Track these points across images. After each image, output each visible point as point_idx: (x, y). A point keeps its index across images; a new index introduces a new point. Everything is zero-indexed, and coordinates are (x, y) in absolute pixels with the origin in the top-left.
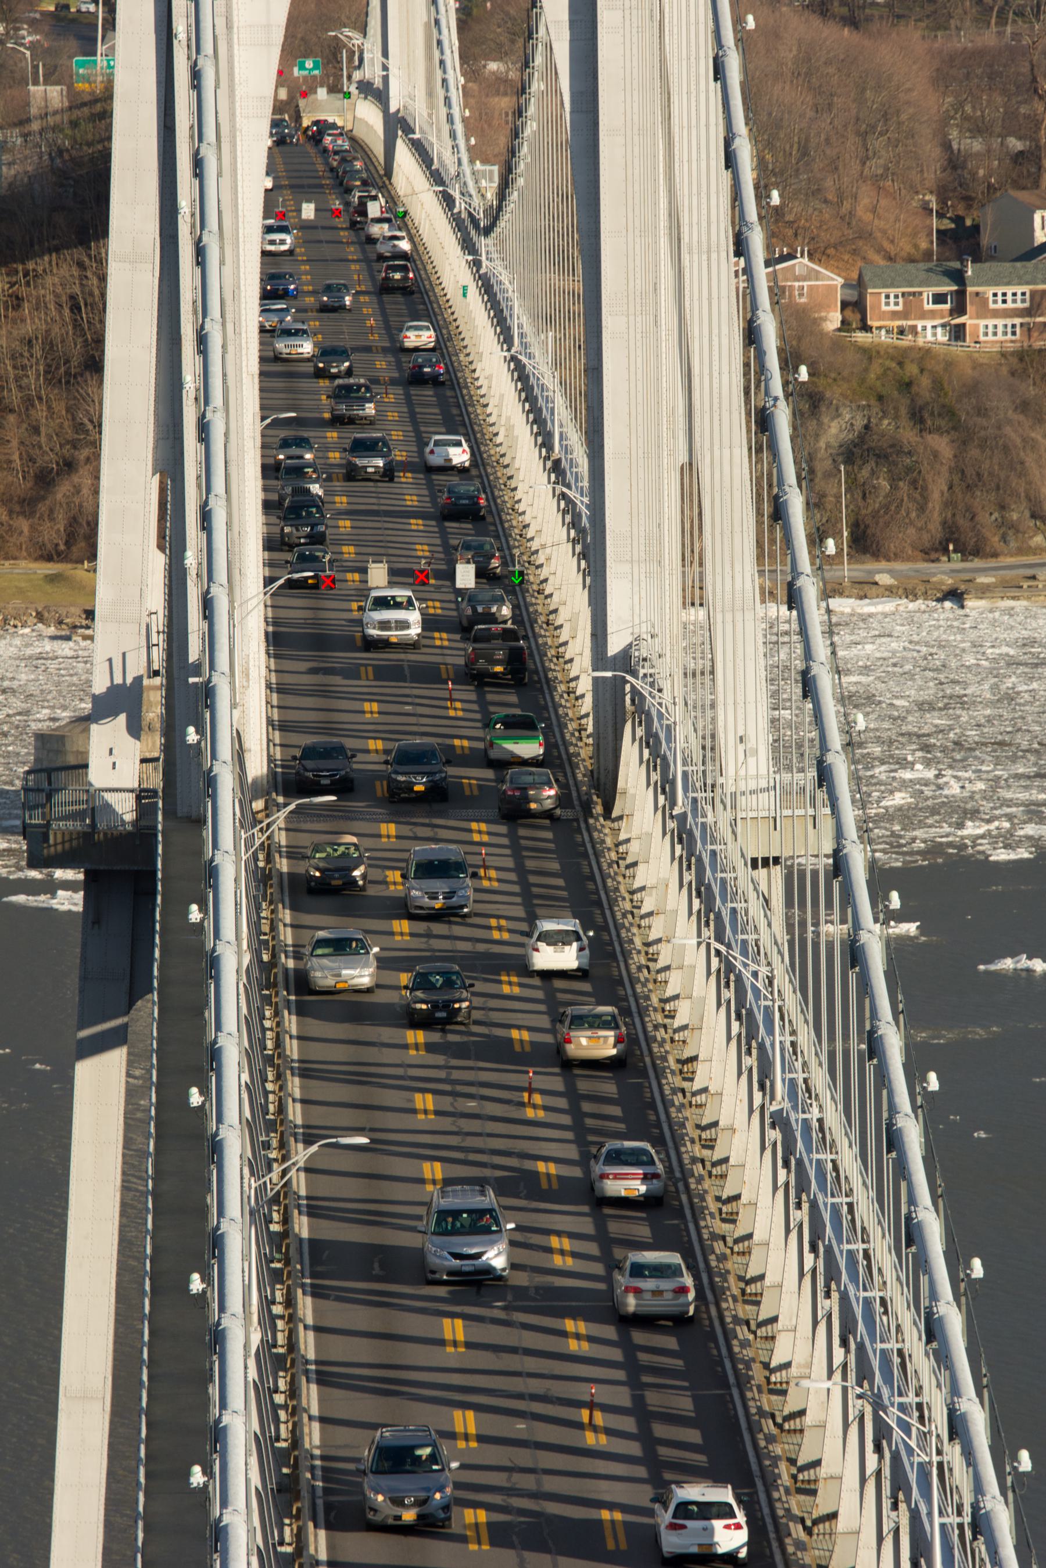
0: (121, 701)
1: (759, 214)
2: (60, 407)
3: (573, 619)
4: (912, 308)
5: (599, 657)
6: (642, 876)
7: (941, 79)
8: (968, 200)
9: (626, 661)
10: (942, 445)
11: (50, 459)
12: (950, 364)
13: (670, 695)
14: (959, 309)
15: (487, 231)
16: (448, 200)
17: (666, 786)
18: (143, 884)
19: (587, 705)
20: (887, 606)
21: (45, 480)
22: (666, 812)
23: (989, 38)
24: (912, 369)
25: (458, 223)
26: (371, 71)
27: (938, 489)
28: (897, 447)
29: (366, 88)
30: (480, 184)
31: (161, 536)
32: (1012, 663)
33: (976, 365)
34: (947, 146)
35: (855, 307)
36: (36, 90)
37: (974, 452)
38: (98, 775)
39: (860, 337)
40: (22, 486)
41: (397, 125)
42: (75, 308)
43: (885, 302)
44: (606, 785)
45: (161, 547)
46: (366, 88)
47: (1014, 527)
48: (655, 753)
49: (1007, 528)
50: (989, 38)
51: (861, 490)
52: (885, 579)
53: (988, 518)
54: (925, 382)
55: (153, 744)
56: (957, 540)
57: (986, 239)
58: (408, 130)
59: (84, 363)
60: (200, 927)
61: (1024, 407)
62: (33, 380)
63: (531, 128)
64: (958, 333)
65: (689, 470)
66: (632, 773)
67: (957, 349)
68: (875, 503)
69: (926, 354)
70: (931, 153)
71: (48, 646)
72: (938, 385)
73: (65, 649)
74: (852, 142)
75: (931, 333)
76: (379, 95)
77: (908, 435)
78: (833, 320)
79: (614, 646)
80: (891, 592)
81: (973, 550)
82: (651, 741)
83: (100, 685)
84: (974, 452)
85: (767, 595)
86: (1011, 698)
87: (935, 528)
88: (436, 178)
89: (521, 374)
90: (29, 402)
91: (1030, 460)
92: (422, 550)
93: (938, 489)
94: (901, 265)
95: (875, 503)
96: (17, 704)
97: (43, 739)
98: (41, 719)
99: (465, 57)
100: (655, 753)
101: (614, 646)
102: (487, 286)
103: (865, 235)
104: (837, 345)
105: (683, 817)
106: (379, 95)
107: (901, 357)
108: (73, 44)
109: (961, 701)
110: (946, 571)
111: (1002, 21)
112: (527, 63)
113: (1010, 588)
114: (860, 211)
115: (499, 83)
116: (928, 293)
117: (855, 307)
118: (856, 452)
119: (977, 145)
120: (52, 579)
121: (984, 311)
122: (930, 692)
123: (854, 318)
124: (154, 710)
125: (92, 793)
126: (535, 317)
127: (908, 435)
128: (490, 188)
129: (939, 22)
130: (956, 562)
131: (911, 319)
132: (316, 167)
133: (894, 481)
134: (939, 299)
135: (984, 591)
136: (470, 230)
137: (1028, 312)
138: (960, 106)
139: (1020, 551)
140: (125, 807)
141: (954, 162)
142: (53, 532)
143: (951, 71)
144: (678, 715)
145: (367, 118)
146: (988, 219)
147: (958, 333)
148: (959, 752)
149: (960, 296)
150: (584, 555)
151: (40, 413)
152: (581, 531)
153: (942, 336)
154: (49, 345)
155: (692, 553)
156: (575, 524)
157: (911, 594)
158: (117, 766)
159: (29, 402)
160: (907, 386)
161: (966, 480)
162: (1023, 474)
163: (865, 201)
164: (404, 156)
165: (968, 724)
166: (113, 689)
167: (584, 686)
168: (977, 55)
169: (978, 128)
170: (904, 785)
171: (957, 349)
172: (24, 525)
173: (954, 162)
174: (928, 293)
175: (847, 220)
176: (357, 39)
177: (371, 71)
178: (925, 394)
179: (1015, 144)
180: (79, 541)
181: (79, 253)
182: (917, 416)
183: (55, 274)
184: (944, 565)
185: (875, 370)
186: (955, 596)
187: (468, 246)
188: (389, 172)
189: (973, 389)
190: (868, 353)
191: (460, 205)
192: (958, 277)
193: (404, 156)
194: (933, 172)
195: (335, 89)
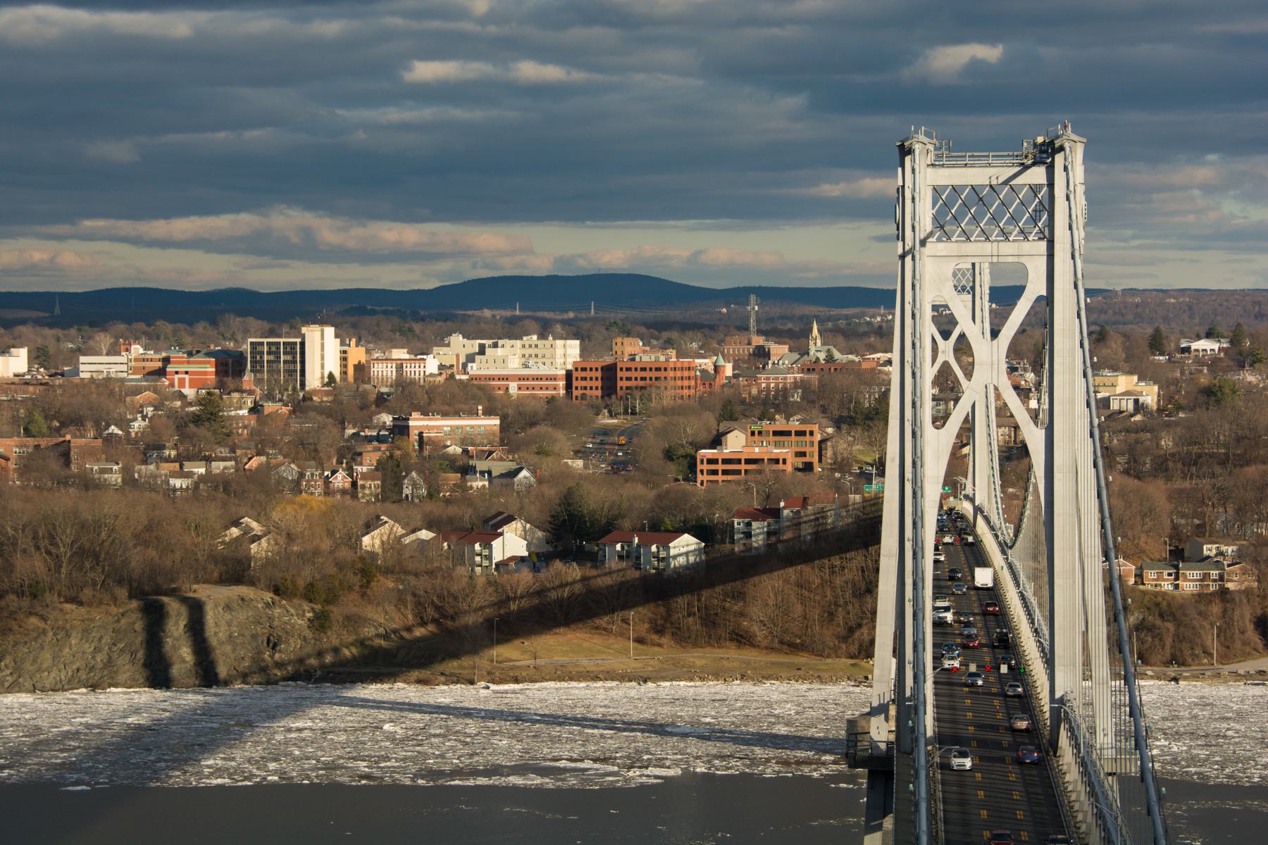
0: (882, 709)
1: (28, 691)
2: (857, 605)
3: (1042, 685)
4: (1160, 578)
5: (1052, 699)
6: (1068, 778)
7: (1170, 498)
8: (1180, 541)
9: (1062, 701)
10: (1170, 626)
11: (853, 624)
12: (1173, 598)
13: (1078, 710)
14: (1177, 578)
15: (1011, 548)
16: (996, 536)
17: (1077, 746)
18: (889, 775)
19: (1047, 715)
20: (1151, 682)
21: (851, 630)
22: (1077, 755)
23: (1187, 484)
24: (1160, 599)
25: (1000, 544)
26: (969, 491)
27: (1169, 641)
28: (1154, 626)
29: (966, 497)
30: (1008, 531)
31: (894, 651)
32: (1196, 704)
33: (1183, 598)
34: (1172, 521)
35: (1139, 576)
36: (851, 496)
37: (1182, 629)
38: (874, 735)
39: (1141, 587)
40: (842, 631)
41: (978, 510)
42: (863, 571)
43: (1150, 575)
44: (1054, 745)
45: (894, 656)
46: (966, 497)
47: (1197, 656)
48: (1073, 734)
49: (1194, 656)
50: (1187, 484)
51: (1142, 641)
52: (1150, 673)
53: (1187, 652)
54: (1165, 603)
55: (892, 725)
56: (1176, 659)
57: (1186, 554)
58: (982, 512)
59: (870, 588)
60: (914, 793)
61: (1200, 614)
62: (848, 595)
63: (1027, 513)
64: (1176, 587)
65: (1085, 634)
66: (1064, 740)
67: (1176, 592)
68: (1147, 646)
69: (1165, 594)
70: (1167, 523)
71: (851, 689)
72: (1169, 605)
73: (857, 690)
74: (1139, 518)
75: (1167, 586)
76: (972, 500)
77: (1158, 622)
78: (1132, 581)
79: (1058, 695)
80: (1152, 677)
81: (1182, 663)
82: (1071, 730)
83: (875, 704)
84: (1182, 629)
85: (1115, 676)
86: (1196, 717)
87: (1168, 656)
88: (992, 528)
89: (1023, 598)
90: (846, 603)
91: (1202, 632)
92: (987, 659)
93: (1169, 641)
94: (1158, 562)
95: (1147, 646)
96: (841, 709)
97: (849, 722)
98: (849, 714)
99: (1002, 486)
100: (1073, 734)
101: (1058, 695)
102: (1011, 567)
103: (1143, 552)
104: (1133, 589)
105: (1083, 758)
106: (972, 500)
107: (1156, 594)
108: (864, 480)
109: (1177, 717)
110: (1172, 671)
111: (1191, 478)
112: (1027, 490)
113: (1195, 677)
114: (1141, 543)
115: (1015, 496)
116: (1166, 572)
117: (1139, 576)
118: (1139, 627)
119: (1183, 521)
120: (853, 665)
121: (1186, 580)
122: (1166, 714)
123: (1139, 580)
124: (893, 711)
125: (872, 741)
126: (1028, 578)
127: (1158, 622)
128: (1011, 532)
129: (1169, 479)
130: (1176, 668)
131: (1160, 581)
132: (952, 522)
133: (1153, 638)
134: (1170, 575)
135: (1185, 679)
136: (1004, 547)
137: (1201, 580)
138: (1176, 508)
139: (1200, 664)
140: (883, 746)
141: (1175, 527)
142: (854, 649)
143: (1177, 496)
144: (1080, 720)
145: (967, 508)
146: (1187, 547)
147: (1176, 587)
148: (1177, 736)
149: (1177, 574)
150: (1046, 662)
151: (850, 607)
152: (1045, 654)
153: (1171, 588)
154: (854, 585)
155: (1087, 663)
156: (1043, 651)
157: (1159, 678)
158: (881, 732)
159: (846, 603)
160: (1157, 605)
161: (1179, 638)
162: (1200, 637)
163: (1143, 540)
164: (980, 520)
165: (1181, 726)
166: (880, 705)
167: (1046, 708)
168: (1181, 491)
169: (1183, 516)
170: (1157, 747)
171: (1176, 592)
172: (844, 646)
173: (1175, 527)
174: (1166, 572)
175: (1137, 546)
176: (964, 480)
177: (969, 491)
178: (1164, 608)
179: (1197, 522)
180: (867, 650)
181: (864, 551)
182: (1162, 616)
183: (856, 559)
184: (1171, 668)
185: (1147, 599)
186: (1176, 680)
187: (1004, 552)
188: (975, 525)
189: (1182, 607)
190: (1144, 593)
191: (1001, 538)
192: (1176, 567)
193: (980, 520)
194: (1168, 531)
195: (955, 497)
